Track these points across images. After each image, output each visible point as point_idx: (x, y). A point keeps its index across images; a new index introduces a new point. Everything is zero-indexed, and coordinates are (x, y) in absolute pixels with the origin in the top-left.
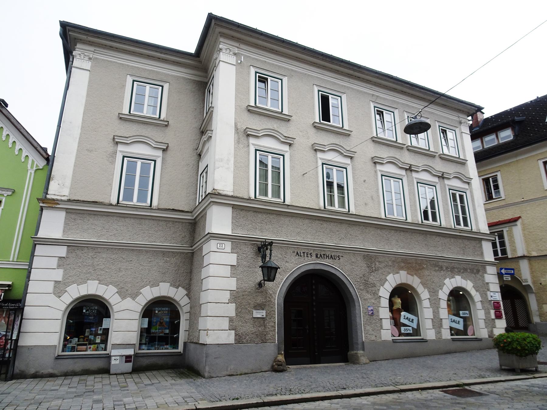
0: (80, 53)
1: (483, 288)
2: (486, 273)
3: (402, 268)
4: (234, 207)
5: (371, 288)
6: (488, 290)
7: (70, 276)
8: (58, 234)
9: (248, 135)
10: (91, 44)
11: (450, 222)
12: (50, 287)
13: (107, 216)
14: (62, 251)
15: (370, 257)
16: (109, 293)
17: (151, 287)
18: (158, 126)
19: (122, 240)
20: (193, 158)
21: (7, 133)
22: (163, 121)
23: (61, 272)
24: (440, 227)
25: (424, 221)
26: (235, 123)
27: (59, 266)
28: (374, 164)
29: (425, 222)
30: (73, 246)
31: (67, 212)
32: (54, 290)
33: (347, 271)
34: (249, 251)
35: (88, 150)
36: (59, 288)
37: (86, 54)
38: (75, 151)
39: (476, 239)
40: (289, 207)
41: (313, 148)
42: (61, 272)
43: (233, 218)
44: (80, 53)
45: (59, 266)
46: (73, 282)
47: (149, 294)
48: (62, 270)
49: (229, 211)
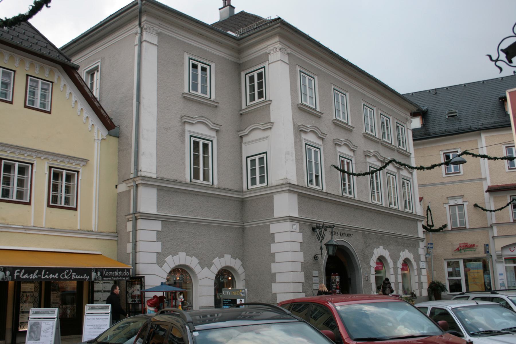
0: (150, 26)
1: (417, 258)
2: (419, 247)
3: (380, 244)
4: (300, 195)
5: (367, 258)
6: (420, 260)
7: (167, 248)
8: (154, 211)
9: (336, 144)
10: (157, 17)
11: (304, 181)
12: (153, 258)
13: (185, 193)
14: (158, 226)
15: (366, 234)
16: (192, 262)
17: (219, 258)
18: (210, 106)
19: (197, 216)
20: (68, 91)
21: (76, 99)
22: (213, 101)
23: (159, 244)
24: (353, 199)
25: (310, 185)
26: (293, 119)
27: (158, 239)
28: (334, 145)
29: (310, 185)
30: (165, 220)
31: (157, 189)
32: (157, 261)
33: (354, 244)
34: (309, 231)
35: (165, 129)
36: (160, 261)
37: (154, 28)
38: (156, 129)
39: (413, 219)
40: (328, 195)
41: (334, 142)
42: (159, 244)
43: (299, 203)
44: (150, 26)
45: (158, 239)
46: (169, 254)
47: (219, 264)
48: (160, 243)
49: (295, 198)
